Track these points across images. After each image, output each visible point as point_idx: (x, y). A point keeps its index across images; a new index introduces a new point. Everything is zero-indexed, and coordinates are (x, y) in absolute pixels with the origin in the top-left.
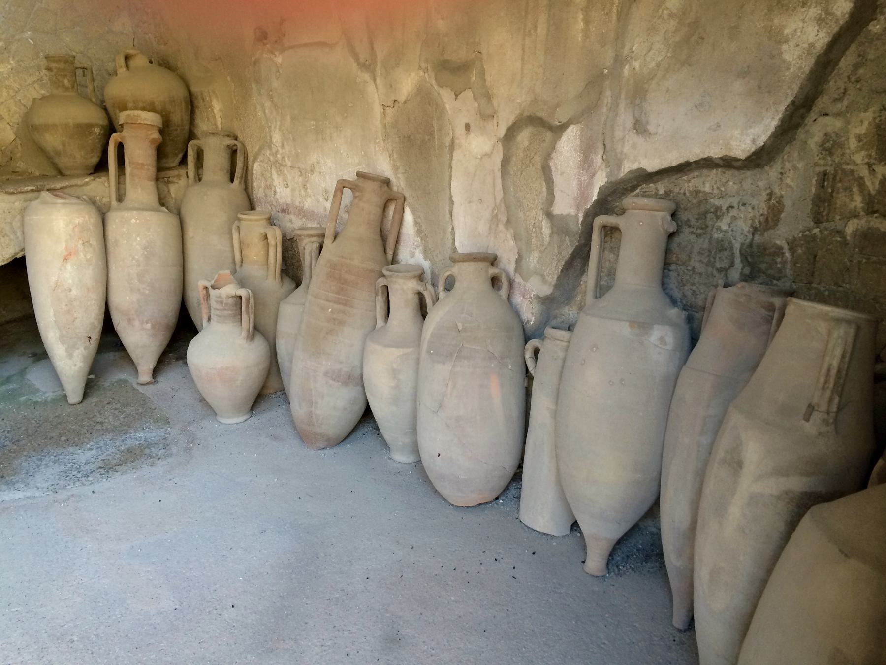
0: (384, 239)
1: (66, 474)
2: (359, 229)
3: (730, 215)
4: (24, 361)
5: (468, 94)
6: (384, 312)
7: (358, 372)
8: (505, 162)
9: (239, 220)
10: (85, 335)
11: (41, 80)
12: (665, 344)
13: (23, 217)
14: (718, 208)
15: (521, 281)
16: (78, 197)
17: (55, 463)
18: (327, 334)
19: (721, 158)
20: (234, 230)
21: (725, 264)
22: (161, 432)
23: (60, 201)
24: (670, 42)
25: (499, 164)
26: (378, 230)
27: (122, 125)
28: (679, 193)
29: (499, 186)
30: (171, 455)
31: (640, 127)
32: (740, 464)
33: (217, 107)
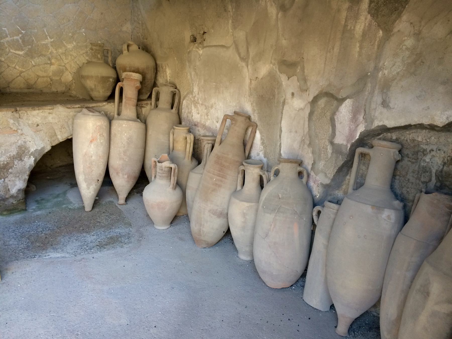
0: (244, 145)
2: (234, 139)
3: (431, 154)
4: (66, 187)
5: (295, 78)
7: (226, 211)
8: (311, 114)
9: (174, 129)
13: (73, 119)
14: (425, 150)
15: (314, 175)
16: (100, 112)
18: (212, 191)
19: (429, 125)
20: (171, 133)
21: (426, 179)
22: (127, 230)
23: (91, 114)
24: (405, 62)
25: (308, 115)
27: (123, 79)
28: (404, 140)
29: (306, 126)
31: (385, 104)
33: (168, 72)
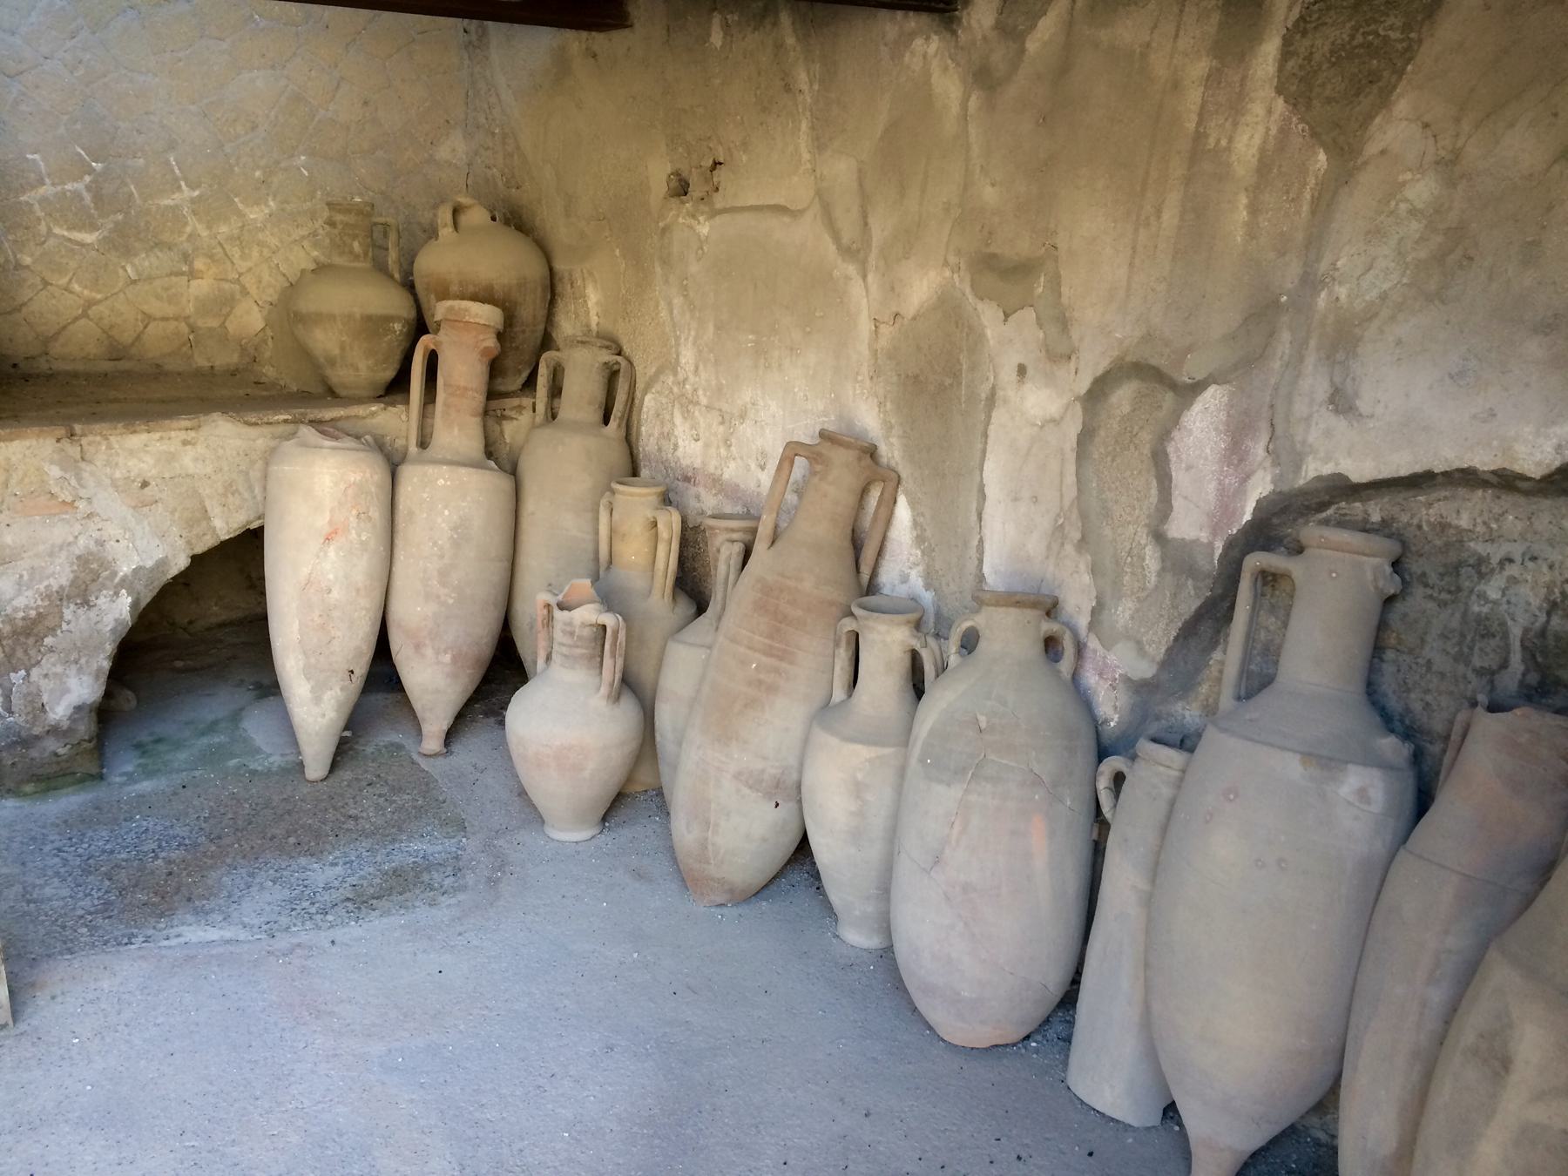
0: (857, 545)
1: (291, 904)
2: (819, 526)
5: (1028, 315)
6: (848, 676)
7: (795, 776)
8: (1085, 437)
9: (613, 492)
10: (347, 667)
11: (315, 234)
12: (1368, 801)
13: (267, 464)
15: (1099, 647)
16: (358, 437)
17: (274, 882)
18: (746, 706)
19: (1494, 472)
21: (1491, 661)
22: (450, 845)
23: (328, 443)
24: (1409, 259)
25: (1074, 440)
26: (849, 532)
27: (438, 324)
29: (1070, 478)
30: (463, 888)
31: (1341, 402)
32: (1506, 1064)
33: (593, 297)
